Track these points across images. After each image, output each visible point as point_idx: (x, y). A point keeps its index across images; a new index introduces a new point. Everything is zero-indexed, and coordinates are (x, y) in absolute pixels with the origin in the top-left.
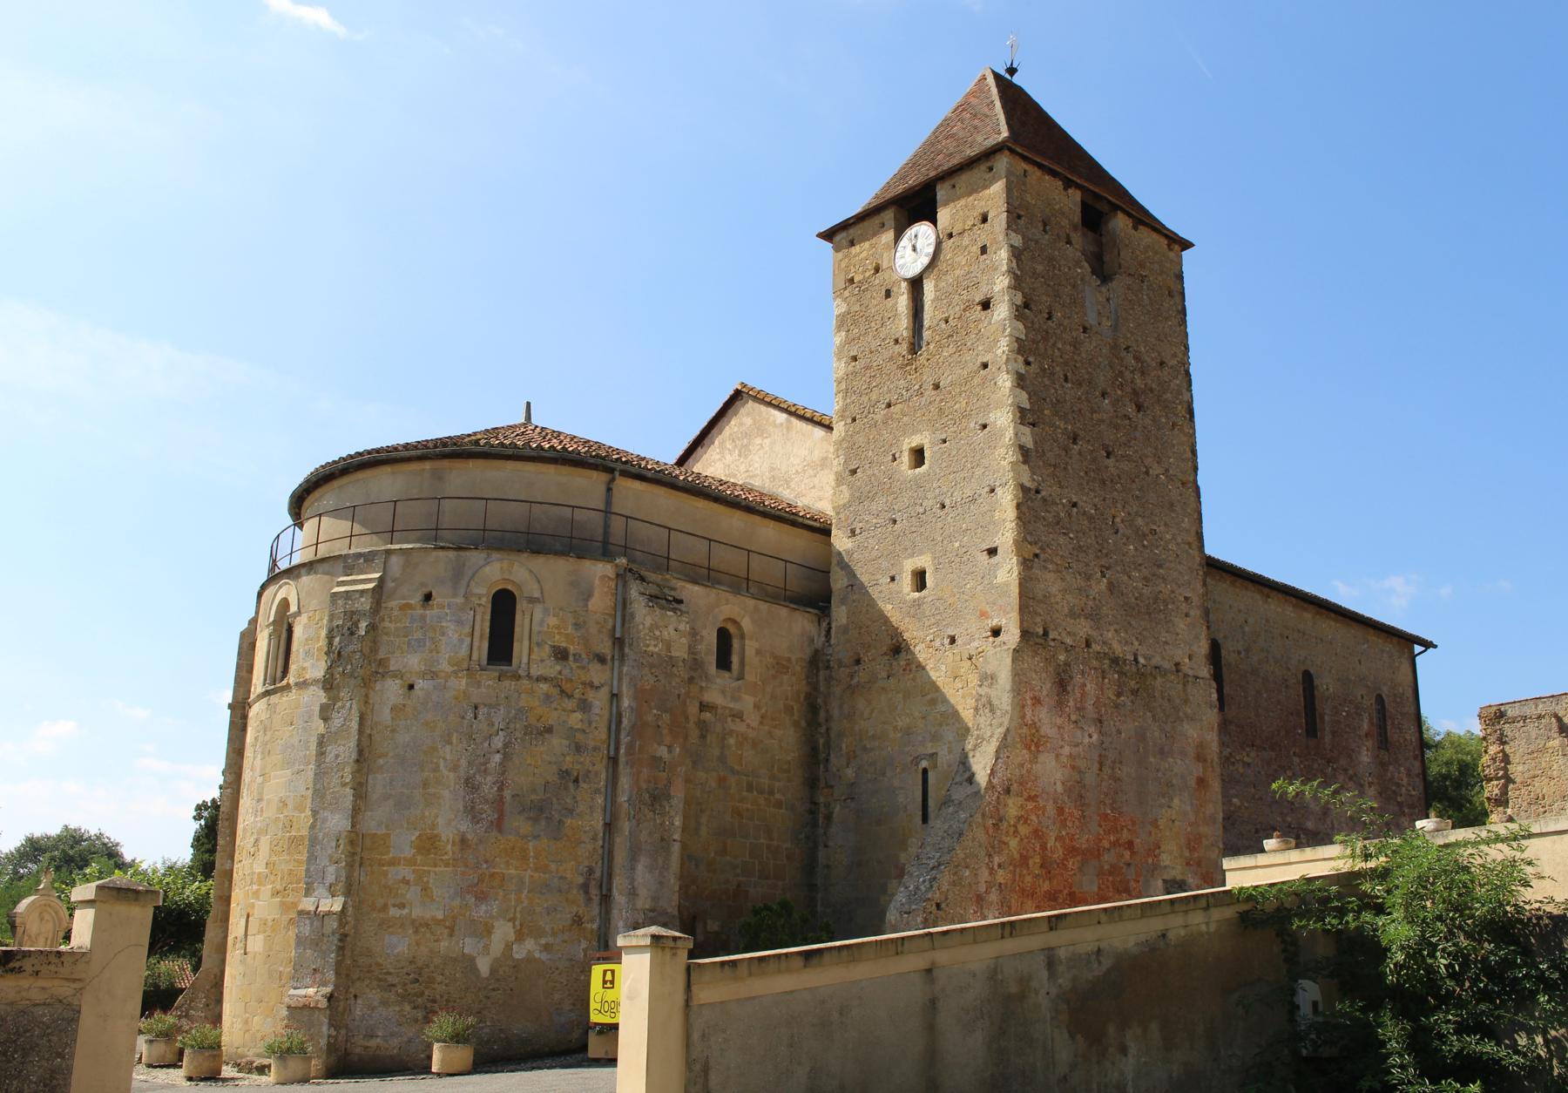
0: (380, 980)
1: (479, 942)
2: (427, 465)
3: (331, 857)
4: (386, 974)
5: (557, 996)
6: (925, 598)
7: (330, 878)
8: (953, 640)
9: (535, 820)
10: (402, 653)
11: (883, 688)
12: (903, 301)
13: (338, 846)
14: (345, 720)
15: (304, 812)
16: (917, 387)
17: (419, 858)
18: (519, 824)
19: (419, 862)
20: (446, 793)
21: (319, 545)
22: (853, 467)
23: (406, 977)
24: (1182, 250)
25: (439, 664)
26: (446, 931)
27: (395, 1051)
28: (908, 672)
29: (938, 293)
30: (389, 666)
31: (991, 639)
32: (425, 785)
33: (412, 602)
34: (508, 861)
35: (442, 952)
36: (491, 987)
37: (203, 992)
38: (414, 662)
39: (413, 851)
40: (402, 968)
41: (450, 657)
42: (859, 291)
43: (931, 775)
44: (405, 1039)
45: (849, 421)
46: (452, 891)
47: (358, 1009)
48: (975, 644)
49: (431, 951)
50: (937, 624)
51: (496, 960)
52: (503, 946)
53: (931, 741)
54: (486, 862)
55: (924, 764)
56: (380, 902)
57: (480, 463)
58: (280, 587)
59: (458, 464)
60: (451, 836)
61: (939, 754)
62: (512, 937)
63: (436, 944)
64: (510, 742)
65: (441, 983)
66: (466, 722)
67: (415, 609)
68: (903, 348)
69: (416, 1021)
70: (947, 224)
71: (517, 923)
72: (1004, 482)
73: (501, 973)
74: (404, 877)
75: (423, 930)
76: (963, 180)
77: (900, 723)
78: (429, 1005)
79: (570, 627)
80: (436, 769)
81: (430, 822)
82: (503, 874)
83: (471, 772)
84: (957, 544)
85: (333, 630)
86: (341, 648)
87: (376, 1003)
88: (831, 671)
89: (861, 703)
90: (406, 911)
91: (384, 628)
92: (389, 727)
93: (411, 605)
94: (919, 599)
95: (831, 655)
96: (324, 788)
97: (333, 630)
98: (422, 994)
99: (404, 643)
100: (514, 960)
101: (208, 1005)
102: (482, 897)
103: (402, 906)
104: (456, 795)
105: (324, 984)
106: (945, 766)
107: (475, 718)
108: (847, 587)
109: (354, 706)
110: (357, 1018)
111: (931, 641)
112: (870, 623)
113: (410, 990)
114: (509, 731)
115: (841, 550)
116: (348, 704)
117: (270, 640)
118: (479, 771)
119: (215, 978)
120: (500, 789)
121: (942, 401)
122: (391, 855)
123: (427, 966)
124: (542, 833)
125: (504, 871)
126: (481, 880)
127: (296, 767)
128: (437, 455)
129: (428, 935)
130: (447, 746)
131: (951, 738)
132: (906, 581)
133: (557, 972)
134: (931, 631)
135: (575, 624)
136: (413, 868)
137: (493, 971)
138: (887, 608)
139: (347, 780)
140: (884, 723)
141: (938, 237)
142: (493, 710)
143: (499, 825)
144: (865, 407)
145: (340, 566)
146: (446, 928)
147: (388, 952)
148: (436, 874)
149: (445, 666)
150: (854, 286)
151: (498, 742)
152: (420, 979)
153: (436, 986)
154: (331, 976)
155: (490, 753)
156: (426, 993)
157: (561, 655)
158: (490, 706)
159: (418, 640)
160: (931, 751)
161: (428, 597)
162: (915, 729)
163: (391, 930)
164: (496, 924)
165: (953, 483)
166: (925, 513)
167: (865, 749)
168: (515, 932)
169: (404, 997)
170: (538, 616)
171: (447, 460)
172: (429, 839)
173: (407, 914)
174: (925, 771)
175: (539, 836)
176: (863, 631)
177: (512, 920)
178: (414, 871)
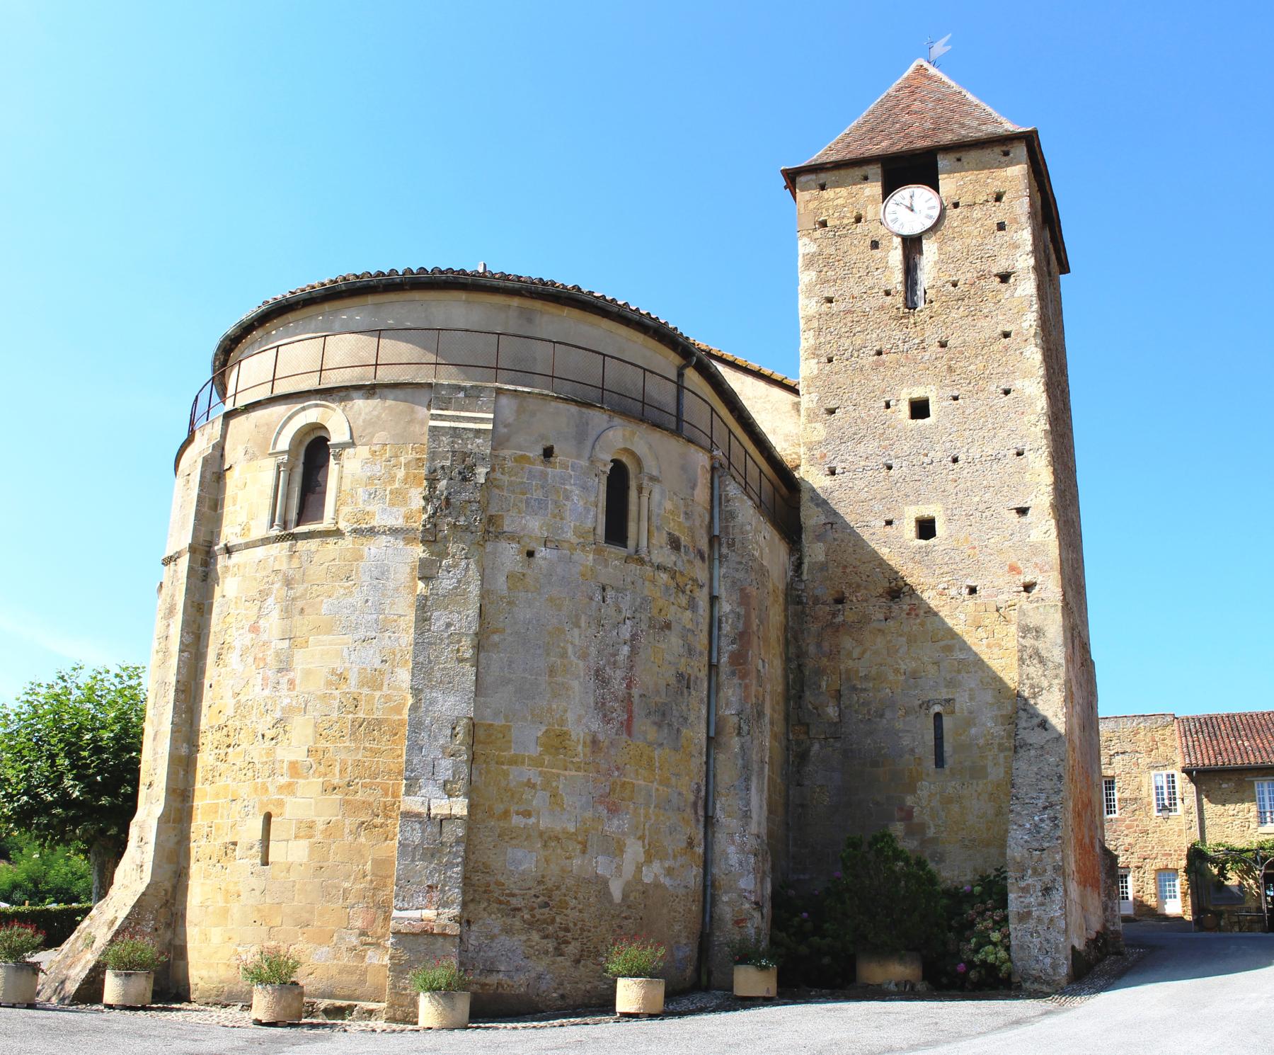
0: (500, 902)
1: (612, 861)
2: (515, 302)
3: (444, 748)
4: (508, 895)
5: (677, 928)
6: (934, 546)
7: (445, 772)
8: (973, 590)
9: (659, 725)
10: (519, 512)
11: (879, 630)
12: (895, 256)
13: (454, 736)
14: (459, 581)
16: (917, 341)
17: (547, 758)
18: (645, 728)
19: (546, 762)
20: (575, 684)
21: (374, 363)
22: (831, 406)
23: (534, 899)
24: (1061, 273)
25: (563, 532)
26: (579, 847)
28: (913, 616)
29: (942, 256)
30: (503, 527)
31: (1024, 594)
32: (552, 671)
34: (637, 770)
35: (574, 871)
36: (623, 915)
37: (151, 912)
38: (534, 525)
39: (539, 749)
40: (530, 889)
41: (575, 527)
42: (835, 235)
43: (947, 723)
44: (533, 975)
45: (824, 359)
46: (584, 799)
47: (473, 937)
48: (1005, 597)
49: (563, 870)
50: (952, 572)
51: (628, 883)
52: (634, 868)
53: (946, 686)
54: (618, 769)
55: (937, 708)
56: (499, 808)
57: (576, 313)
58: (303, 409)
59: (551, 308)
60: (582, 735)
61: (957, 700)
62: (642, 858)
63: (568, 861)
64: (636, 634)
66: (594, 604)
67: (533, 464)
68: (899, 300)
69: (546, 953)
70: (953, 192)
71: (646, 842)
72: (1036, 447)
73: (632, 898)
74: (529, 780)
75: (553, 844)
76: (973, 155)
77: (903, 667)
79: (682, 516)
80: (564, 655)
81: (558, 716)
82: (634, 784)
83: (601, 662)
84: (977, 499)
85: (435, 471)
86: (450, 494)
87: (496, 931)
88: (804, 607)
89: (847, 643)
90: (532, 820)
91: (495, 479)
92: (505, 597)
93: (529, 458)
95: (802, 591)
96: (430, 662)
97: (435, 471)
98: (553, 921)
99: (521, 501)
100: (644, 884)
101: (156, 930)
102: (613, 810)
103: (527, 814)
104: (586, 688)
105: (445, 904)
106: (966, 714)
107: (604, 602)
109: (472, 566)
110: (471, 948)
111: (944, 589)
112: (858, 564)
113: (538, 916)
114: (636, 620)
115: (815, 486)
116: (463, 563)
117: (279, 473)
118: (608, 662)
119: (166, 894)
120: (629, 687)
121: (951, 359)
123: (558, 888)
124: (665, 742)
125: (634, 782)
126: (613, 790)
127: (361, 633)
128: (531, 293)
129: (559, 851)
130: (575, 629)
131: (973, 686)
133: (677, 900)
134: (944, 579)
135: (686, 513)
136: (540, 769)
137: (625, 897)
138: (884, 552)
139: (467, 655)
141: (942, 203)
142: (621, 595)
143: (628, 726)
144: (846, 350)
145: (425, 395)
146: (579, 843)
147: (512, 868)
148: (566, 779)
149: (570, 535)
150: (827, 229)
151: (626, 630)
152: (551, 903)
153: (568, 911)
154: (455, 894)
155: (619, 644)
156: (558, 919)
157: (675, 544)
158: (618, 590)
159: (539, 501)
161: (548, 453)
162: (923, 674)
163: (513, 842)
164: (627, 842)
165: (970, 440)
166: (931, 463)
167: (854, 688)
168: (644, 852)
169: (531, 924)
170: (656, 496)
171: (540, 302)
173: (533, 823)
174: (938, 716)
175: (662, 744)
176: (848, 570)
177: (642, 838)
178: (540, 773)
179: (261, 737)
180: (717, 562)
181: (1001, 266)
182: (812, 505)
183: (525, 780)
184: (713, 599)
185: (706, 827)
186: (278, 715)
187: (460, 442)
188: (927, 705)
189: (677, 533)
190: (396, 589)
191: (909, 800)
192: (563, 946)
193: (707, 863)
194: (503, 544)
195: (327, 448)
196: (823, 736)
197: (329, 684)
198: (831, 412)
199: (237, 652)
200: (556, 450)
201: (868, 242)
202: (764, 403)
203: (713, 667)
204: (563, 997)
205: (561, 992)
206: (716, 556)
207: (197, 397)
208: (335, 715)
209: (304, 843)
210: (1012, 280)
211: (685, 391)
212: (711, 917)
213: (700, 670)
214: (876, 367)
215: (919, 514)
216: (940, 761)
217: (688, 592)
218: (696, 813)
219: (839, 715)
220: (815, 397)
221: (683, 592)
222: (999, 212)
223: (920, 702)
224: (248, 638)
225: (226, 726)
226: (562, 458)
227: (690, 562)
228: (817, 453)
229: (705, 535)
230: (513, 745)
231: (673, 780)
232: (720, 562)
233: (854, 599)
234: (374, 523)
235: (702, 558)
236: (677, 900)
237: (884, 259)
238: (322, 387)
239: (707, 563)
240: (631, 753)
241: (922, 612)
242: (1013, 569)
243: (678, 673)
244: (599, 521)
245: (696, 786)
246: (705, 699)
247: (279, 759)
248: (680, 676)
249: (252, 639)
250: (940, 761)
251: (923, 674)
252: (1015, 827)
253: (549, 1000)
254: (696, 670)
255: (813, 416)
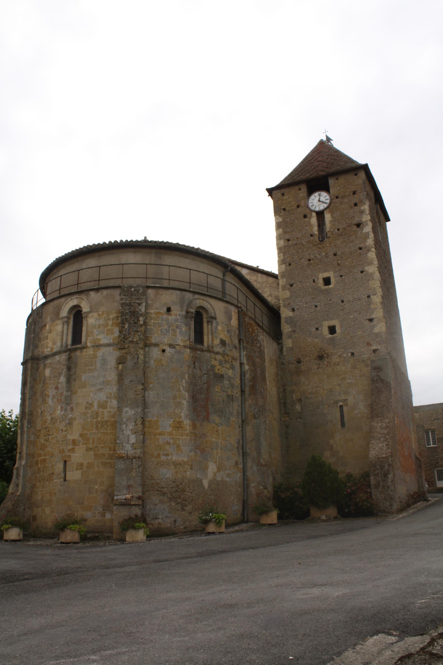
12: (314, 220)
15: (106, 409)
17: (174, 432)
19: (174, 434)
27: (169, 525)
31: (373, 354)
32: (175, 397)
33: (162, 311)
39: (171, 429)
40: (170, 485)
43: (345, 409)
45: (287, 264)
51: (210, 481)
55: (341, 403)
56: (156, 454)
62: (215, 470)
65: (189, 492)
71: (217, 464)
75: (178, 467)
78: (184, 502)
79: (226, 332)
80: (179, 390)
87: (157, 502)
93: (161, 313)
94: (333, 337)
98: (180, 498)
107: (195, 368)
108: (291, 331)
122: (160, 430)
123: (181, 484)
132: (326, 331)
137: (210, 486)
140: (317, 387)
146: (189, 465)
153: (186, 493)
156: (182, 497)
160: (344, 398)
161: (169, 310)
162: (334, 390)
164: (209, 464)
168: (217, 468)
172: (178, 423)
174: (341, 407)
177: (215, 462)
179: (61, 431)
180: (242, 350)
181: (356, 220)
182: (286, 324)
183: (166, 441)
184: (241, 364)
185: (243, 456)
186: (67, 421)
187: (133, 308)
188: (336, 402)
189: (224, 339)
190: (111, 369)
191: (331, 442)
192: (184, 507)
193: (244, 471)
194: (152, 348)
195: (81, 315)
196: (295, 418)
197: (86, 408)
198: (292, 285)
199: (51, 397)
200: (172, 308)
201: (303, 215)
202: (266, 284)
203: (242, 391)
204: (185, 528)
205: (184, 526)
206: (242, 347)
207: (33, 298)
208: (89, 420)
209: (79, 472)
210: (361, 226)
211: (227, 282)
212: (247, 493)
213: (237, 393)
214: (309, 265)
215: (336, 326)
216: (343, 424)
217: (230, 362)
218: (238, 451)
219: (301, 409)
220: (285, 280)
221: (229, 362)
222: (355, 199)
223: (334, 401)
224: (54, 392)
225: (48, 427)
226: (174, 312)
227: (230, 350)
228: (287, 303)
229: (236, 339)
230: (160, 428)
231: (228, 439)
232: (243, 350)
233: (305, 361)
234: (101, 343)
235: (236, 348)
236: (232, 487)
237: (309, 222)
238: (79, 290)
239: (238, 350)
240: (209, 428)
241: (332, 365)
242: (369, 344)
243: (227, 395)
244: (191, 336)
245: (238, 440)
246: (240, 405)
247: (68, 439)
248: (228, 396)
249: (56, 392)
250: (343, 424)
251: (334, 390)
252: (372, 449)
253: (180, 529)
254: (235, 393)
255: (284, 288)
